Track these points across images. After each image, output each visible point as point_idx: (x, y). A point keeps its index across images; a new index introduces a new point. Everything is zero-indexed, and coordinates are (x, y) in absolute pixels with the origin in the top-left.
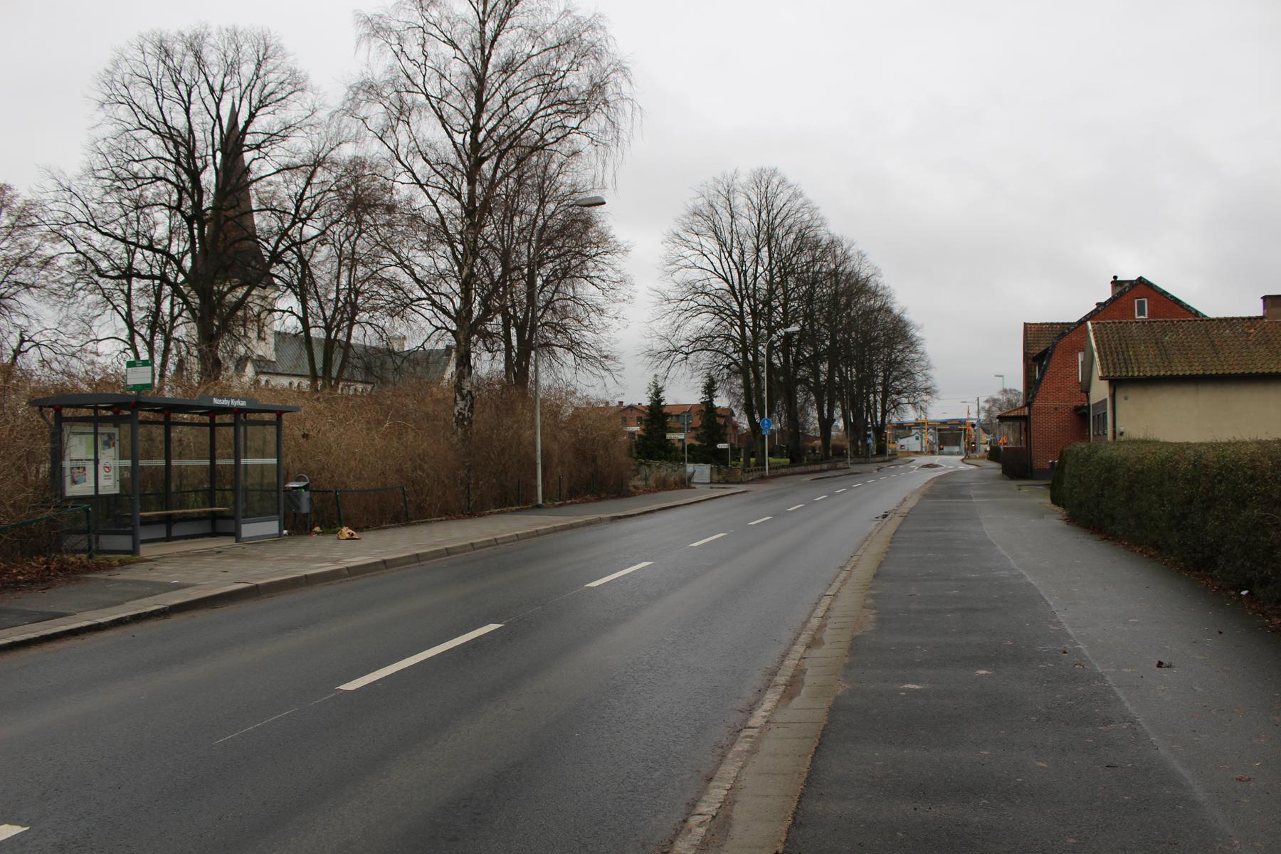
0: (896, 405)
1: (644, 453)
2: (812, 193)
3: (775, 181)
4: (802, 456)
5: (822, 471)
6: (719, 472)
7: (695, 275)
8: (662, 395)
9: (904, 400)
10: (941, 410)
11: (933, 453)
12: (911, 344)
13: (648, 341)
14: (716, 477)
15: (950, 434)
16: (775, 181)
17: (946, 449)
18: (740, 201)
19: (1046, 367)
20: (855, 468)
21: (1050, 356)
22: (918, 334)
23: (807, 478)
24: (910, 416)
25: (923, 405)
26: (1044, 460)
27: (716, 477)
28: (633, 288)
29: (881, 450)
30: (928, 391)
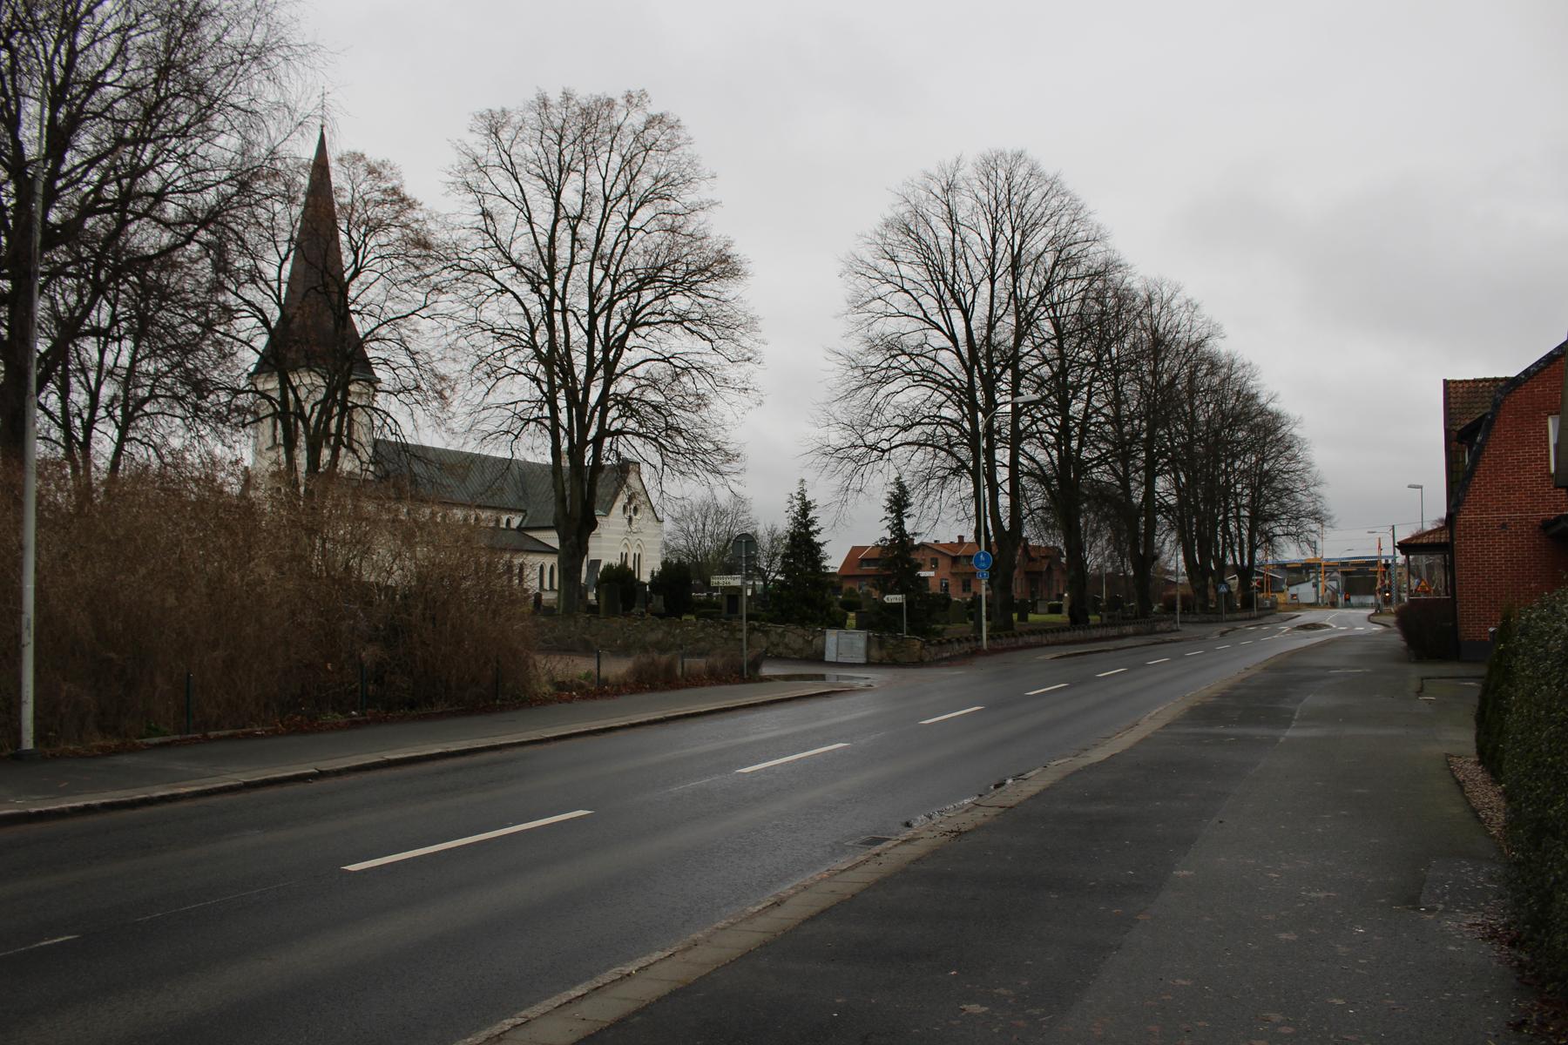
0: (1269, 539)
1: (764, 608)
2: (1076, 183)
3: (1021, 172)
4: (1133, 610)
5: (1122, 636)
6: (881, 645)
7: (890, 326)
8: (811, 514)
9: (1278, 531)
10: (1340, 543)
11: (1334, 605)
12: (1286, 446)
13: (822, 432)
14: (875, 654)
15: (1358, 579)
16: (1021, 172)
17: (1354, 599)
18: (965, 206)
19: (1481, 445)
20: (1190, 630)
21: (1491, 423)
22: (1295, 431)
23: (1047, 655)
24: (1291, 553)
25: (1313, 537)
26: (1479, 626)
27: (875, 654)
28: (759, 336)
29: (1248, 603)
30: (1317, 516)
